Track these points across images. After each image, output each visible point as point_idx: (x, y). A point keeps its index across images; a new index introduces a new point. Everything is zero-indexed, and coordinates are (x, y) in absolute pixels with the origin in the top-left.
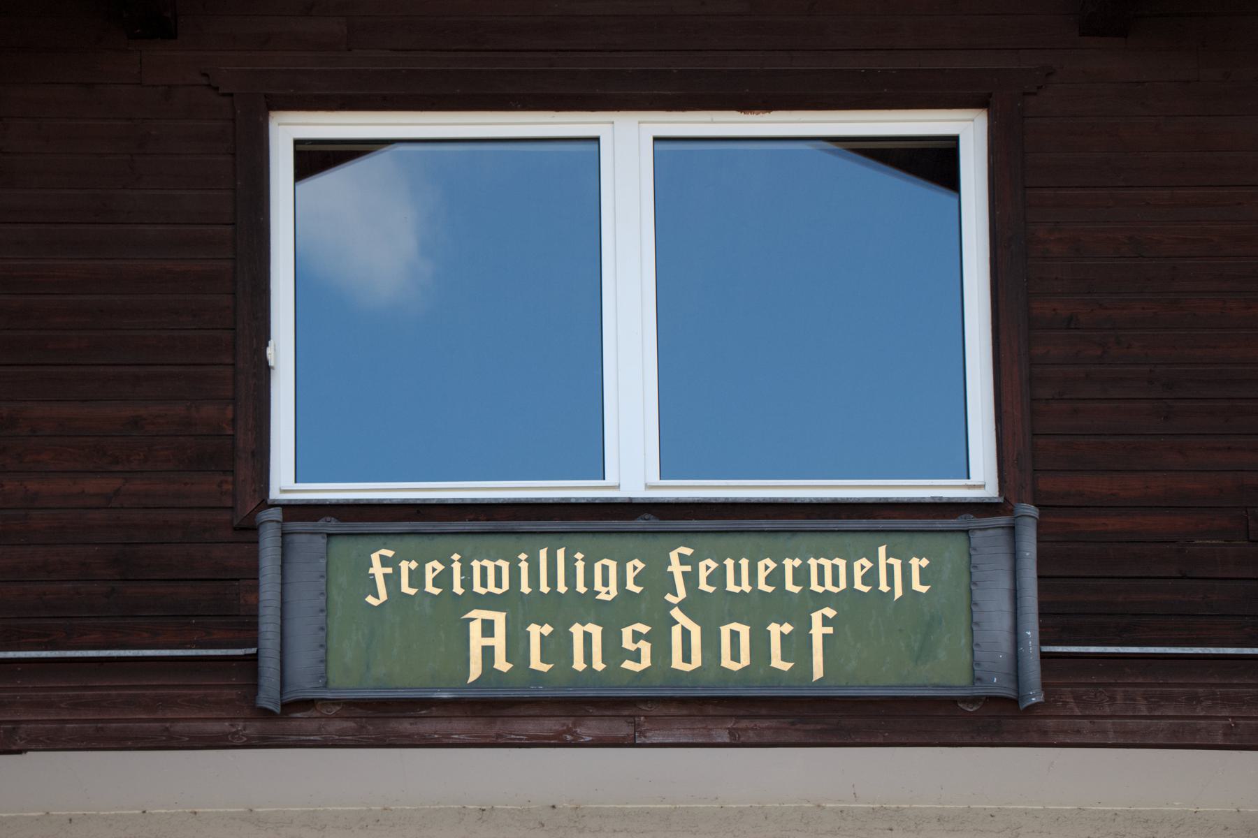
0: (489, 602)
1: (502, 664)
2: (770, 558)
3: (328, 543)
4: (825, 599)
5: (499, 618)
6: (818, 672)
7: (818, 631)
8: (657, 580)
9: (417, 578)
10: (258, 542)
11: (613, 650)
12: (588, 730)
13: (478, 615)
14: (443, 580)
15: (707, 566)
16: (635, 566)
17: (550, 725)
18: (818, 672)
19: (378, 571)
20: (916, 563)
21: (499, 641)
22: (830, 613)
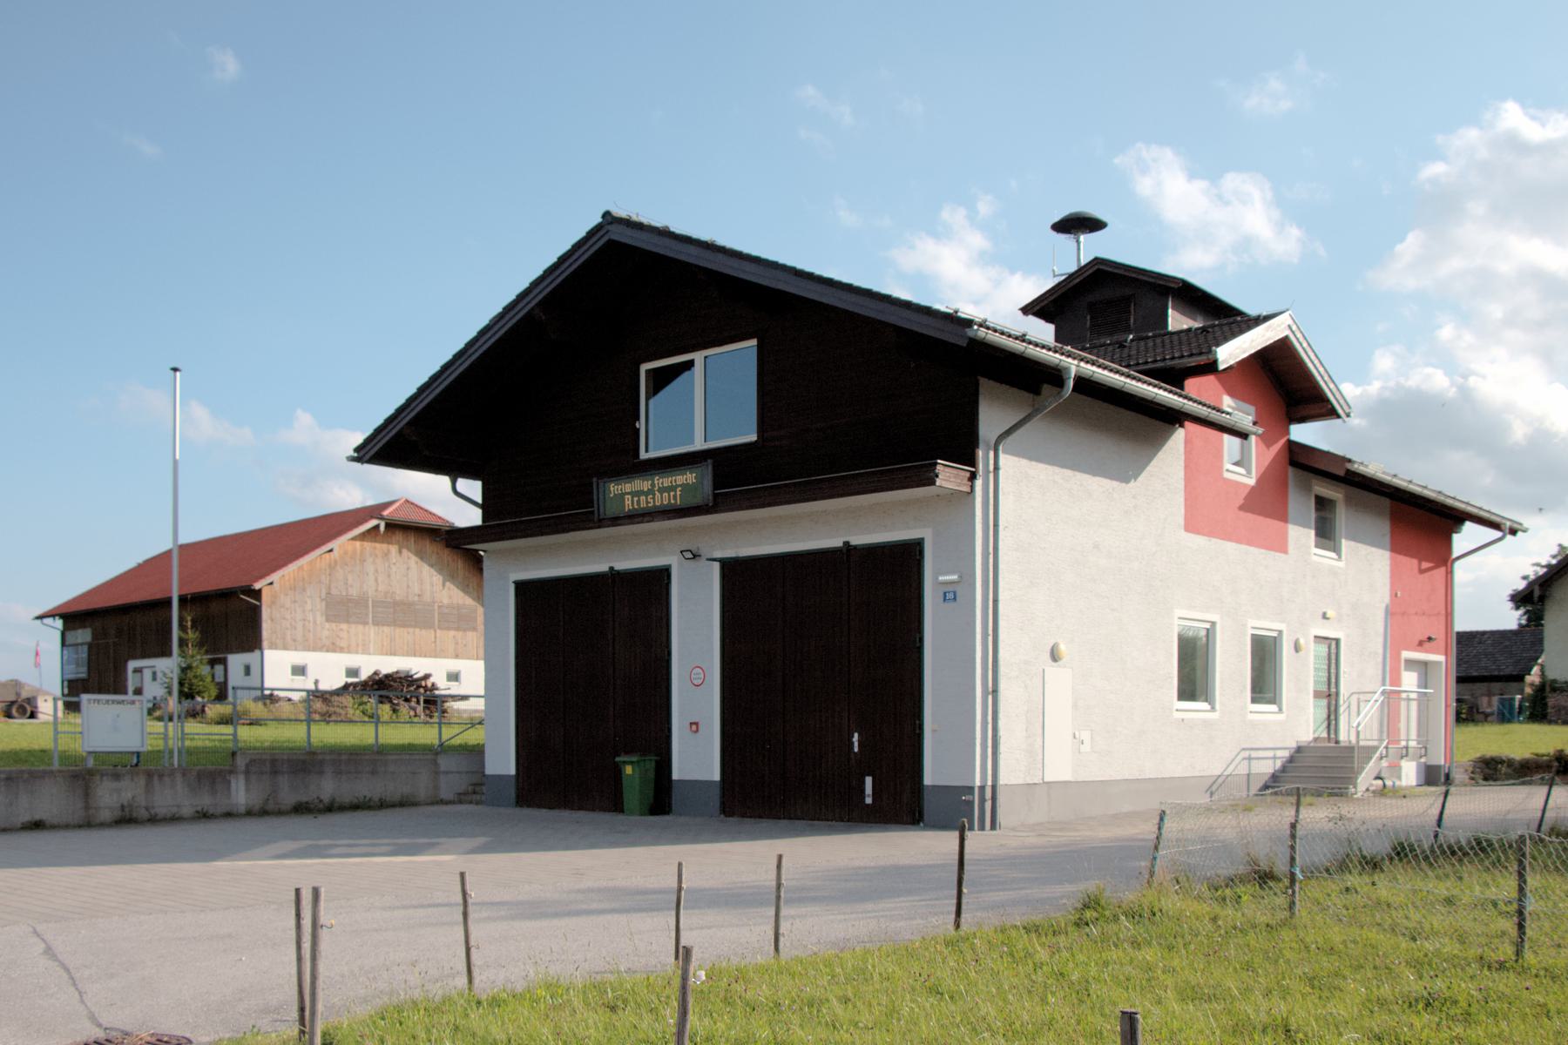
0: (628, 493)
1: (631, 507)
2: (1056, 328)
3: (1250, 770)
4: (628, 493)
5: (629, 497)
6: (678, 502)
7: (678, 493)
8: (653, 485)
9: (638, 502)
10: (1461, 680)
11: (647, 502)
12: (646, 519)
13: (627, 497)
14: (621, 490)
15: (661, 480)
16: (650, 482)
17: (640, 519)
18: (678, 502)
19: (612, 489)
20: (694, 475)
21: (630, 502)
22: (680, 488)
